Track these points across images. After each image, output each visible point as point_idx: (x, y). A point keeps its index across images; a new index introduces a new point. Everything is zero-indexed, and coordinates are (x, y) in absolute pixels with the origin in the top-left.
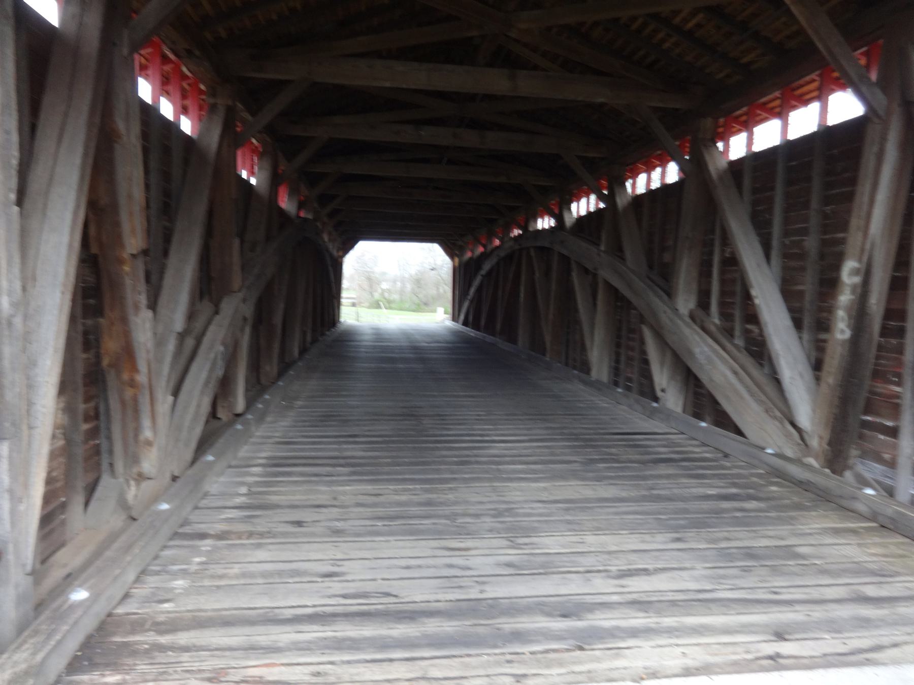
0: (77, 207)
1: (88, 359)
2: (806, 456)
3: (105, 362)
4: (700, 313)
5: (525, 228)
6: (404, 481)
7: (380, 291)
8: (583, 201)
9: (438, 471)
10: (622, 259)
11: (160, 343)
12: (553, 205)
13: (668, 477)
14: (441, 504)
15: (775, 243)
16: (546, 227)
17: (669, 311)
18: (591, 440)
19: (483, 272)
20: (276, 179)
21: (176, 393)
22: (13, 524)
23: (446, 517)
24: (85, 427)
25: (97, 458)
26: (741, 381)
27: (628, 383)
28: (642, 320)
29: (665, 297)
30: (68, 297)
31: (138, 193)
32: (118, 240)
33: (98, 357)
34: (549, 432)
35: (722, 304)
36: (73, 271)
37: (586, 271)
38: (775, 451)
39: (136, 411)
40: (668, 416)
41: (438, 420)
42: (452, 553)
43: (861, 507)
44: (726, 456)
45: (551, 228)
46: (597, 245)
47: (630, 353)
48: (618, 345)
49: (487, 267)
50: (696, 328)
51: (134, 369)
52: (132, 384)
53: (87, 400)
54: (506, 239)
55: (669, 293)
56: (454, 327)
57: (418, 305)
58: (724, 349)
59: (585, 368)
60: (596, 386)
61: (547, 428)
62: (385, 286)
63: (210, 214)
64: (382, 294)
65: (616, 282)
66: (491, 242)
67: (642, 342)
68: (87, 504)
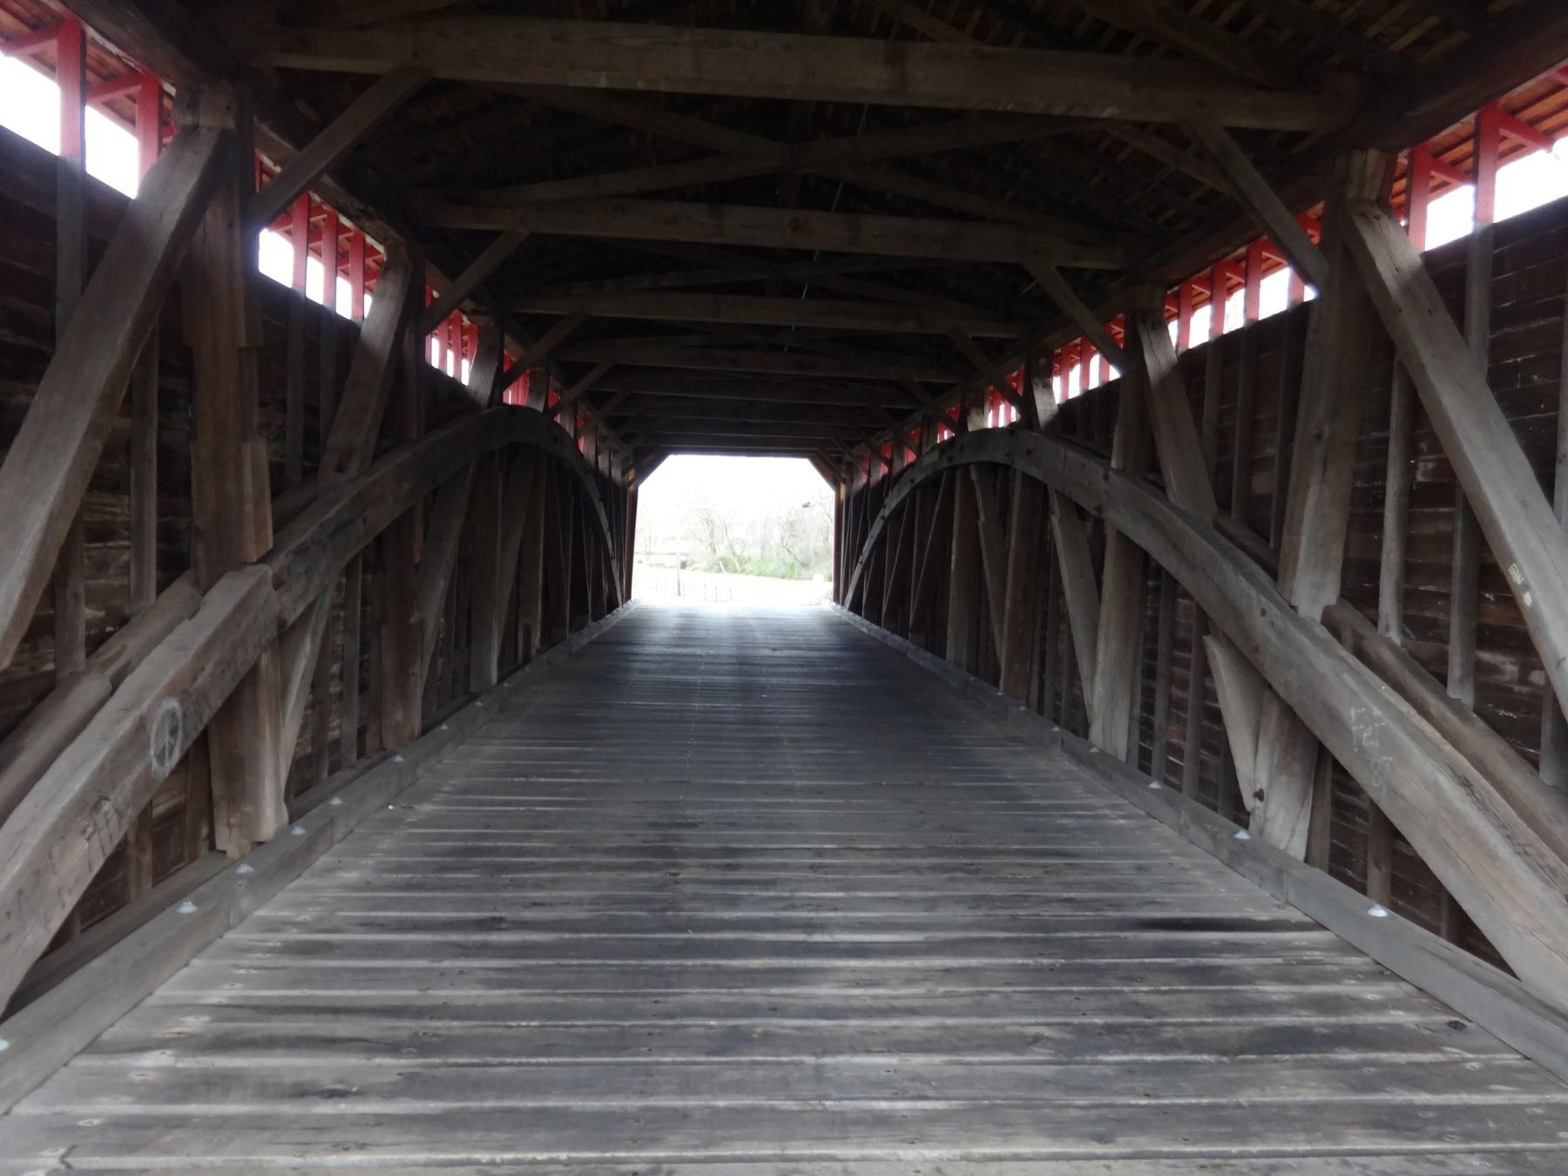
4: (1351, 617)
5: (960, 426)
7: (726, 543)
8: (1075, 373)
9: (647, 1079)
10: (1161, 488)
12: (1015, 380)
13: (1311, 1119)
16: (1002, 423)
17: (1273, 611)
18: (1084, 948)
19: (886, 512)
26: (1483, 806)
27: (1171, 758)
28: (1205, 624)
29: (1264, 577)
34: (979, 914)
35: (1407, 597)
37: (1081, 513)
40: (1271, 866)
41: (718, 867)
45: (1012, 425)
46: (1104, 457)
47: (1177, 692)
48: (1150, 673)
49: (892, 502)
50: (1344, 653)
54: (926, 449)
55: (1274, 567)
56: (838, 614)
57: (792, 566)
58: (1424, 712)
59: (1079, 725)
60: (1101, 764)
61: (978, 901)
64: (731, 546)
65: (1145, 538)
66: (902, 458)
67: (1206, 671)
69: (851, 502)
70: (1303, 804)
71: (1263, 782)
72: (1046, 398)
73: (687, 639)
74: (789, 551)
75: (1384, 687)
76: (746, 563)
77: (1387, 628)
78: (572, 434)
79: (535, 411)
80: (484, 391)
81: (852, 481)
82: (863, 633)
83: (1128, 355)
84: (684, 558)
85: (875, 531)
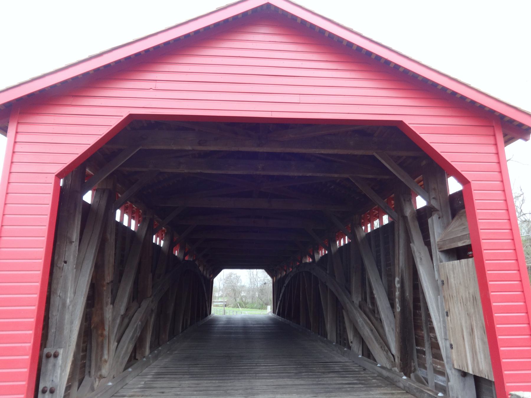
0: (92, 267)
2: (393, 367)
3: (92, 326)
5: (301, 261)
6: (212, 380)
7: (240, 297)
9: (229, 376)
11: (114, 320)
14: (224, 387)
15: (383, 270)
19: (285, 285)
20: (171, 245)
21: (119, 342)
23: (223, 390)
24: (82, 354)
25: (84, 369)
26: (373, 334)
30: (85, 299)
31: (112, 260)
33: (90, 324)
36: (88, 290)
38: (381, 365)
43: (401, 385)
44: (365, 370)
49: (287, 282)
51: (104, 329)
52: (102, 335)
53: (84, 342)
56: (274, 317)
59: (325, 335)
62: (243, 294)
63: (140, 264)
64: (241, 299)
66: (289, 270)
69: (277, 283)
70: (360, 344)
72: (317, 255)
73: (229, 323)
74: (261, 300)
76: (246, 304)
78: (198, 265)
79: (191, 261)
82: (280, 321)
83: (328, 248)
84: (225, 303)
85: (283, 291)
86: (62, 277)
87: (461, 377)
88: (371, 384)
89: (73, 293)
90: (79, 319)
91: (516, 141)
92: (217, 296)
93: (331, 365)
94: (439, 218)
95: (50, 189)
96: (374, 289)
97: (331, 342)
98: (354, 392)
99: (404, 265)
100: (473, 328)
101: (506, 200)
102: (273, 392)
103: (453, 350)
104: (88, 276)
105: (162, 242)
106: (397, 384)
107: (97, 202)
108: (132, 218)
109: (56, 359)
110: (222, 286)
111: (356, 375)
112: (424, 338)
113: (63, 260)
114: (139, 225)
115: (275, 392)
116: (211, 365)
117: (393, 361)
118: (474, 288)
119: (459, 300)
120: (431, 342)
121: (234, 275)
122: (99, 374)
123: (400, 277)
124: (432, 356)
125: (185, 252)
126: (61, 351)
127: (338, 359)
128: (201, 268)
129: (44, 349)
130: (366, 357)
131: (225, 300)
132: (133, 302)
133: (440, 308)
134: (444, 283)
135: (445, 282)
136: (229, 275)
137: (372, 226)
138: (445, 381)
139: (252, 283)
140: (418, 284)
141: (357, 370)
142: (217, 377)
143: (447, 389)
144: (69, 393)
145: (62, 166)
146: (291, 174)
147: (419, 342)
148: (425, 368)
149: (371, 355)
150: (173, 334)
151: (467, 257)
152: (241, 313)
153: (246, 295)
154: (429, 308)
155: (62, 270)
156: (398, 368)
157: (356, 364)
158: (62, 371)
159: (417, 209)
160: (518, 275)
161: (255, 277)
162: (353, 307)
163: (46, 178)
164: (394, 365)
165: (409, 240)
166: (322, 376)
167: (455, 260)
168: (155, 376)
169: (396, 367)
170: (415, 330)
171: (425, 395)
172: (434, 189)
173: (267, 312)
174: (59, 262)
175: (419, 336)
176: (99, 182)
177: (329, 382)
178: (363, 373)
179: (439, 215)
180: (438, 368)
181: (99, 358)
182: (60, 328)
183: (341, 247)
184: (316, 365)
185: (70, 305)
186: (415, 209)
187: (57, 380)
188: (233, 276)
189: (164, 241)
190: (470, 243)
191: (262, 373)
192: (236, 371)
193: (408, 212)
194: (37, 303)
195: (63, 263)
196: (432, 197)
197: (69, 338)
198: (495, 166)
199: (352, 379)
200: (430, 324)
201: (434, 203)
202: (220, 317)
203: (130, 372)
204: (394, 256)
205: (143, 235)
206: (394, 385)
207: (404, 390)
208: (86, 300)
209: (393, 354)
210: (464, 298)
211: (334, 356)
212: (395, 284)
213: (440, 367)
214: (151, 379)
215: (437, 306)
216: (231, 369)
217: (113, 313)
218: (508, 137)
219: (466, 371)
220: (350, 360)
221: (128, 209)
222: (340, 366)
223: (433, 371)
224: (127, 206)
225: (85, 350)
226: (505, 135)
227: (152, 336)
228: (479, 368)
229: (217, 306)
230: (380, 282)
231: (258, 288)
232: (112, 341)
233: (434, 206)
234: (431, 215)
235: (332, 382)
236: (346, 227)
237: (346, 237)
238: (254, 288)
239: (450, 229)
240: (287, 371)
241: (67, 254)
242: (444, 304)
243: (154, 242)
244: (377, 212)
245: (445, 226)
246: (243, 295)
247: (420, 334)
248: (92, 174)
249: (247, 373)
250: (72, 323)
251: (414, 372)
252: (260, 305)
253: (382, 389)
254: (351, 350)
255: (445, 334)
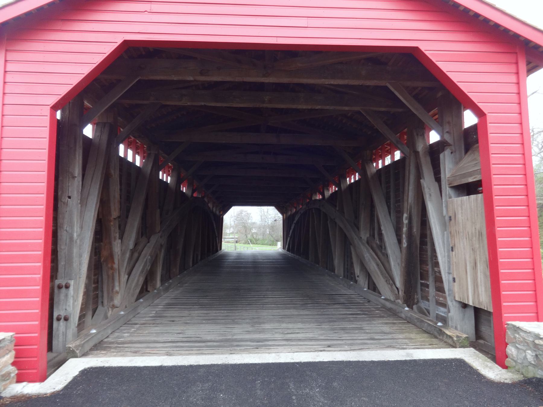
0: (97, 203)
1: (96, 259)
2: (397, 299)
3: (102, 260)
5: (311, 199)
7: (251, 234)
9: (237, 307)
11: (123, 253)
14: (232, 316)
15: (392, 206)
19: (295, 222)
20: (179, 181)
21: (129, 274)
22: (73, 308)
23: (231, 320)
24: (93, 286)
26: (379, 268)
30: (93, 233)
31: (117, 196)
32: (110, 213)
33: (100, 258)
36: (94, 224)
39: (113, 279)
42: (227, 328)
43: (403, 316)
44: (369, 302)
49: (296, 219)
51: (113, 262)
52: (112, 268)
53: (95, 275)
56: (283, 252)
57: (273, 241)
62: (254, 231)
63: (147, 199)
64: (252, 235)
65: (342, 226)
68: (93, 316)
70: (366, 278)
71: (358, 274)
72: (327, 192)
75: (371, 251)
76: (257, 241)
77: (376, 241)
78: (207, 202)
80: (173, 186)
81: (287, 213)
82: (289, 256)
83: (338, 185)
84: (236, 240)
85: (292, 227)
86: (68, 212)
87: (461, 309)
88: (374, 315)
89: (80, 228)
90: (88, 252)
91: (539, 69)
92: (227, 233)
93: (336, 297)
94: (452, 153)
95: (46, 121)
96: (382, 225)
97: (338, 276)
98: (357, 322)
99: (413, 201)
100: (476, 262)
101: (522, 134)
102: (279, 321)
103: (455, 284)
104: (93, 211)
105: (169, 178)
106: (399, 315)
107: (98, 136)
108: (137, 153)
109: (67, 290)
110: (233, 223)
111: (360, 307)
112: (428, 272)
113: (67, 195)
114: (144, 161)
115: (281, 321)
116: (220, 297)
117: (397, 293)
118: (481, 224)
119: (465, 235)
120: (435, 275)
121: (245, 212)
122: (111, 304)
123: (408, 213)
124: (435, 289)
125: (193, 188)
126: (72, 283)
127: (343, 292)
128: (210, 205)
129: (55, 280)
130: (372, 290)
131: (236, 237)
132: (141, 237)
133: (446, 243)
134: (451, 219)
135: (453, 218)
136: (239, 213)
137: (383, 162)
138: (446, 312)
139: (263, 220)
140: (426, 220)
141: (361, 302)
142: (226, 307)
143: (447, 319)
144: (84, 320)
145: (57, 98)
146: (300, 107)
147: (424, 276)
148: (428, 300)
149: (376, 289)
150: (183, 268)
151: (476, 192)
152: (252, 249)
153: (257, 231)
154: (434, 243)
155: (67, 205)
156: (401, 301)
157: (362, 296)
158: (75, 301)
159: (430, 143)
160: (527, 210)
161: (266, 214)
162: (360, 243)
163: (41, 110)
164: (397, 297)
165: (419, 176)
166: (327, 307)
167: (465, 196)
168: (166, 306)
169: (400, 299)
170: (421, 264)
171: (425, 325)
172: (449, 123)
173: (278, 248)
174: (63, 198)
175: (425, 271)
176: (99, 114)
177: (334, 313)
178: (367, 304)
179: (451, 150)
180: (440, 300)
181: (111, 289)
182: (70, 261)
183: (351, 184)
184: (321, 297)
185: (77, 239)
186: (428, 144)
187: (70, 309)
188: (244, 213)
189: (171, 177)
190: (481, 179)
191: (269, 305)
192: (244, 303)
193: (420, 147)
194: (43, 237)
195: (67, 198)
196: (446, 131)
197: (79, 271)
198: (515, 97)
199: (355, 310)
200: (435, 259)
201: (447, 137)
202: (231, 252)
203: (141, 303)
204: (403, 193)
205: (149, 171)
206: (396, 315)
207: (405, 320)
208: (94, 235)
209: (397, 287)
210: (470, 233)
211: (340, 289)
212: (403, 220)
213: (442, 299)
214: (162, 309)
215: (443, 242)
216: (239, 300)
217: (122, 247)
218: (531, 65)
219: (466, 303)
220: (355, 292)
221: (132, 144)
222: (345, 298)
223: (435, 303)
224: (131, 141)
225: (96, 282)
226: (528, 63)
227: (163, 269)
228: (479, 300)
229: (228, 242)
230: (389, 218)
231: (269, 225)
232: (122, 274)
233: (447, 140)
234: (443, 150)
235: (336, 313)
236: (357, 163)
237: (357, 174)
238: (265, 225)
239: (462, 164)
240: (293, 303)
241: (70, 189)
242: (450, 240)
243: (161, 178)
244: (389, 147)
245: (457, 162)
246: (253, 231)
247: (425, 269)
248: (91, 107)
249: (255, 304)
250: (80, 256)
251: (416, 304)
252: (271, 241)
253: (384, 319)
254: (357, 283)
255: (449, 268)
